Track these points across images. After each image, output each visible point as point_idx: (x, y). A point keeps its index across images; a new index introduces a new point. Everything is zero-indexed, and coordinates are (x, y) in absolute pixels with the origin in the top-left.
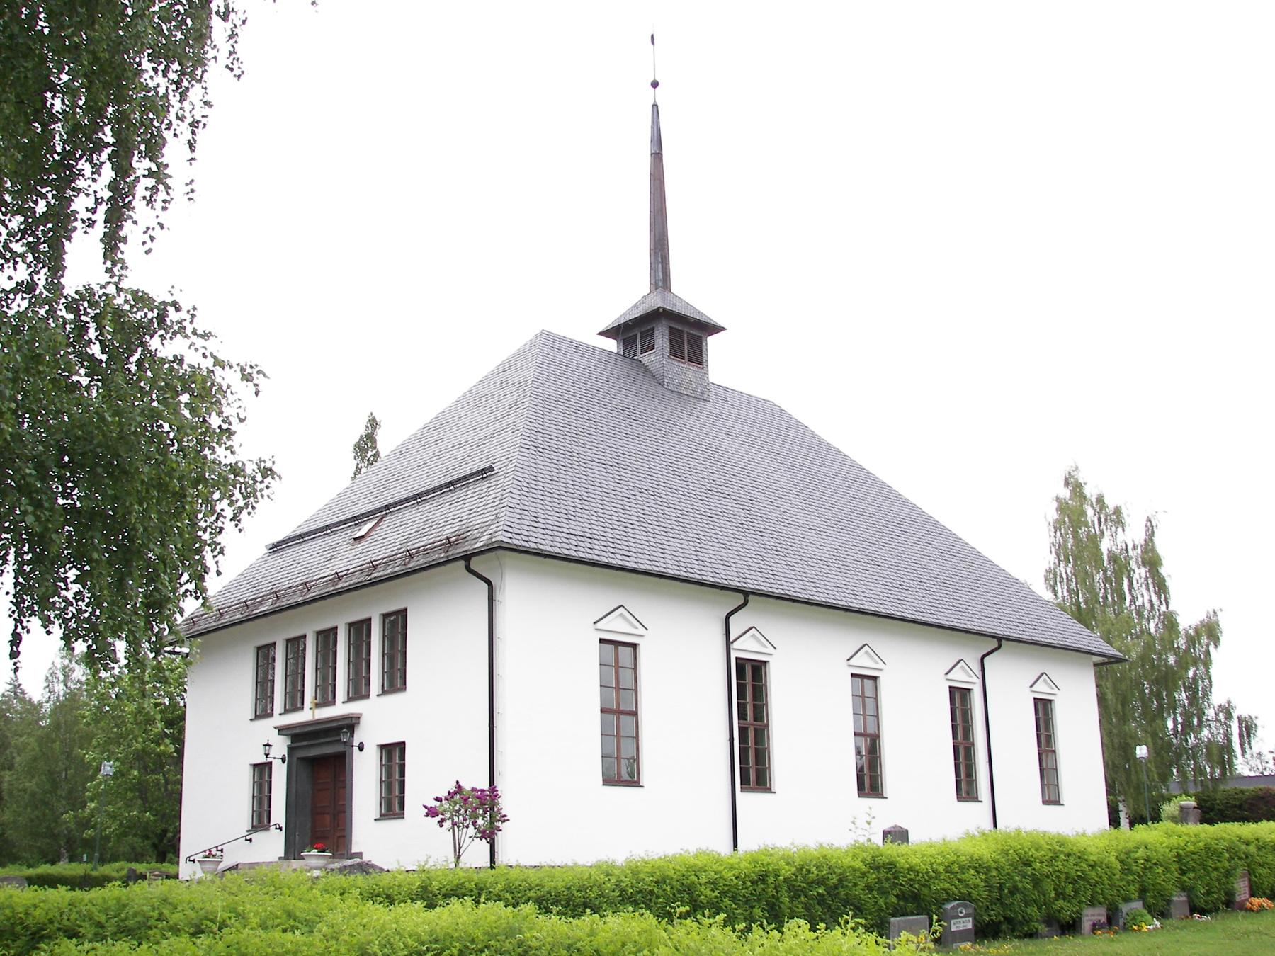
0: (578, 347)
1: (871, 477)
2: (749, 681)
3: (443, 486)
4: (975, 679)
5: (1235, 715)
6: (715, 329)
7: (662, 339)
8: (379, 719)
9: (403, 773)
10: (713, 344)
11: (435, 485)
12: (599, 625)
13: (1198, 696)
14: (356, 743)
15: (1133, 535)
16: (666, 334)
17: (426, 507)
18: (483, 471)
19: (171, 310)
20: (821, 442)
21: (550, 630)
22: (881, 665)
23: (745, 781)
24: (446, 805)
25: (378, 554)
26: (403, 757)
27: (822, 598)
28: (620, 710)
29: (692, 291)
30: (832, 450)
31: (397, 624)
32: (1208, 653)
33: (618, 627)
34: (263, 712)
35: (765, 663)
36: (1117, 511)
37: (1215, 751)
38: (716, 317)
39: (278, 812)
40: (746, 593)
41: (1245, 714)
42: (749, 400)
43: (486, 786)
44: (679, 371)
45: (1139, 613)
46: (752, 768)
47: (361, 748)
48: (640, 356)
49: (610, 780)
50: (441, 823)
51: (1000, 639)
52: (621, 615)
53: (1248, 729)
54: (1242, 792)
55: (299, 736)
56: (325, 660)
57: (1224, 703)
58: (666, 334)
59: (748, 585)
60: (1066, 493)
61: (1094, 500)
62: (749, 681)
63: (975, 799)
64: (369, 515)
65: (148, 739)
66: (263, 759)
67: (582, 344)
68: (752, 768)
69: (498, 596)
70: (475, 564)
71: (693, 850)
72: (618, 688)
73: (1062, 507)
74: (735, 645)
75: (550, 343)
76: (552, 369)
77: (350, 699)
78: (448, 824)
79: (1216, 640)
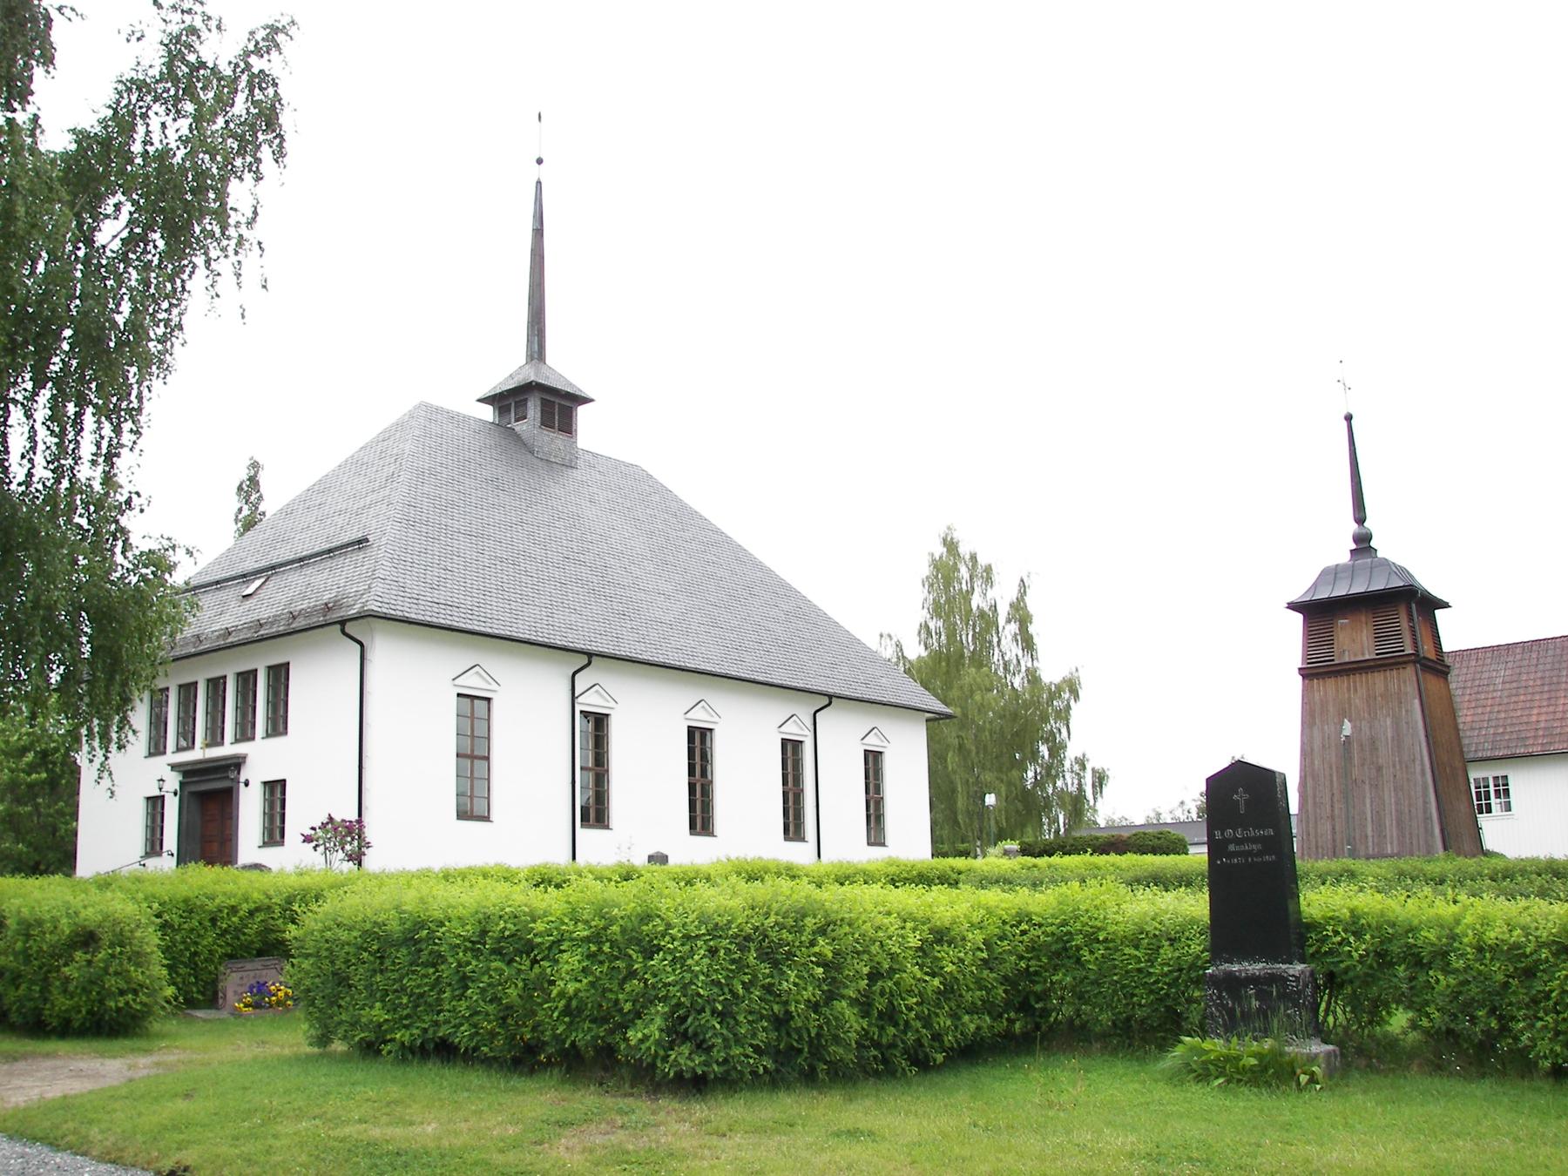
0: (455, 418)
1: (728, 540)
3: (323, 553)
4: (806, 732)
5: (1089, 767)
6: (586, 400)
7: (533, 409)
8: (263, 759)
9: (283, 807)
10: (582, 412)
11: (317, 549)
12: (457, 682)
13: (1057, 749)
14: (242, 779)
15: (1002, 595)
16: (539, 407)
17: (308, 571)
18: (360, 542)
19: (134, 497)
20: (683, 506)
21: (414, 689)
22: (716, 719)
24: (320, 833)
25: (265, 613)
26: (283, 793)
27: (661, 659)
28: (474, 755)
29: (566, 365)
30: (694, 514)
31: (280, 675)
32: (1068, 707)
33: (474, 683)
34: (156, 748)
36: (988, 569)
37: (1067, 799)
38: (585, 389)
40: (590, 655)
41: (1097, 767)
42: (617, 464)
43: (354, 817)
44: (551, 441)
45: (1006, 668)
47: (247, 784)
48: (514, 425)
49: (464, 814)
50: (315, 848)
51: (830, 697)
53: (1100, 780)
54: (1097, 838)
55: (189, 772)
56: (215, 706)
57: (1080, 755)
58: (539, 407)
59: (593, 648)
60: (939, 550)
61: (967, 557)
63: (803, 840)
64: (257, 573)
65: (18, 770)
66: (157, 793)
67: (458, 414)
69: (369, 655)
70: (349, 628)
71: (492, 863)
72: (473, 736)
73: (937, 565)
74: (580, 700)
75: (430, 415)
76: (428, 441)
77: (237, 741)
78: (321, 849)
79: (1075, 693)
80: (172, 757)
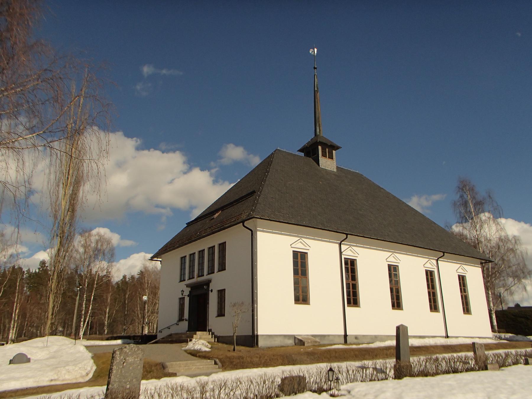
2: (350, 268)
8: (218, 281)
14: (210, 290)
23: (349, 303)
35: (306, 253)
39: (186, 315)
46: (352, 297)
47: (212, 291)
52: (301, 242)
55: (194, 288)
62: (350, 268)
66: (181, 296)
68: (352, 297)
77: (209, 274)
80: (187, 282)
